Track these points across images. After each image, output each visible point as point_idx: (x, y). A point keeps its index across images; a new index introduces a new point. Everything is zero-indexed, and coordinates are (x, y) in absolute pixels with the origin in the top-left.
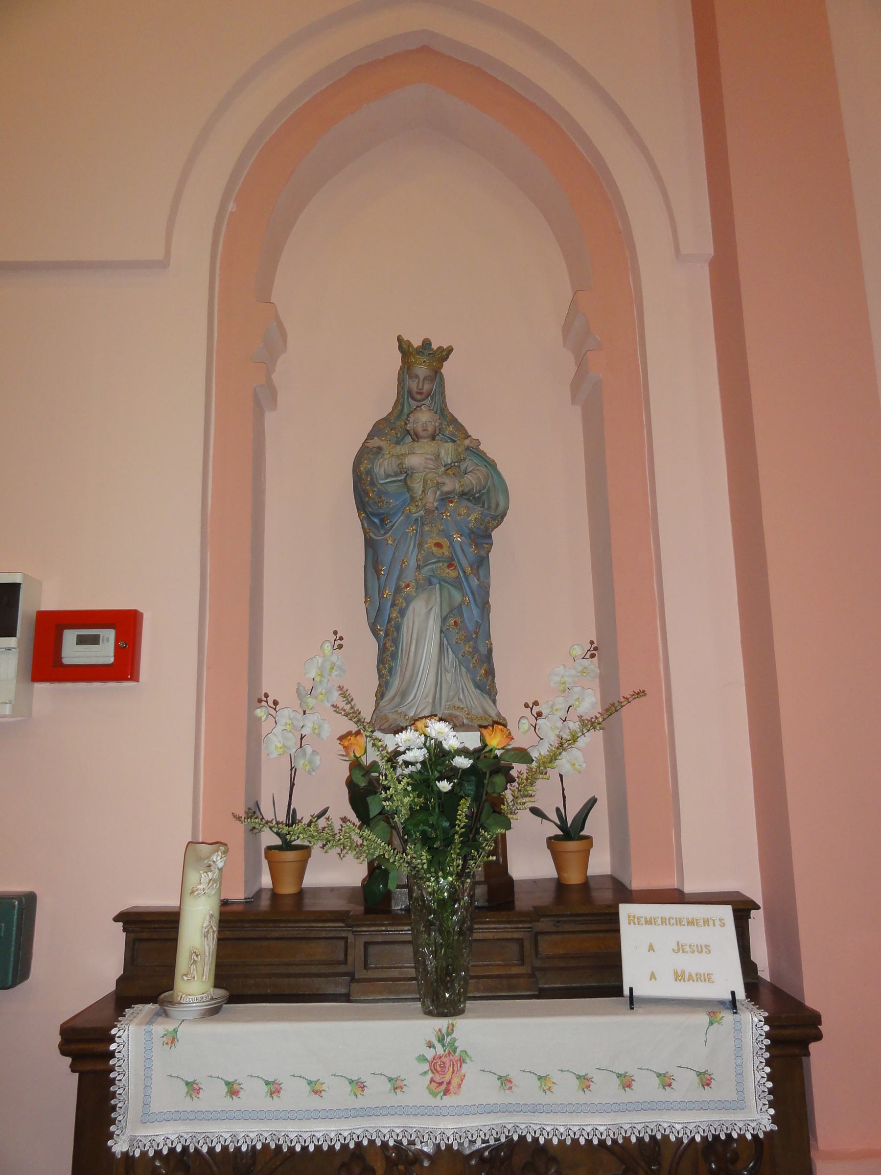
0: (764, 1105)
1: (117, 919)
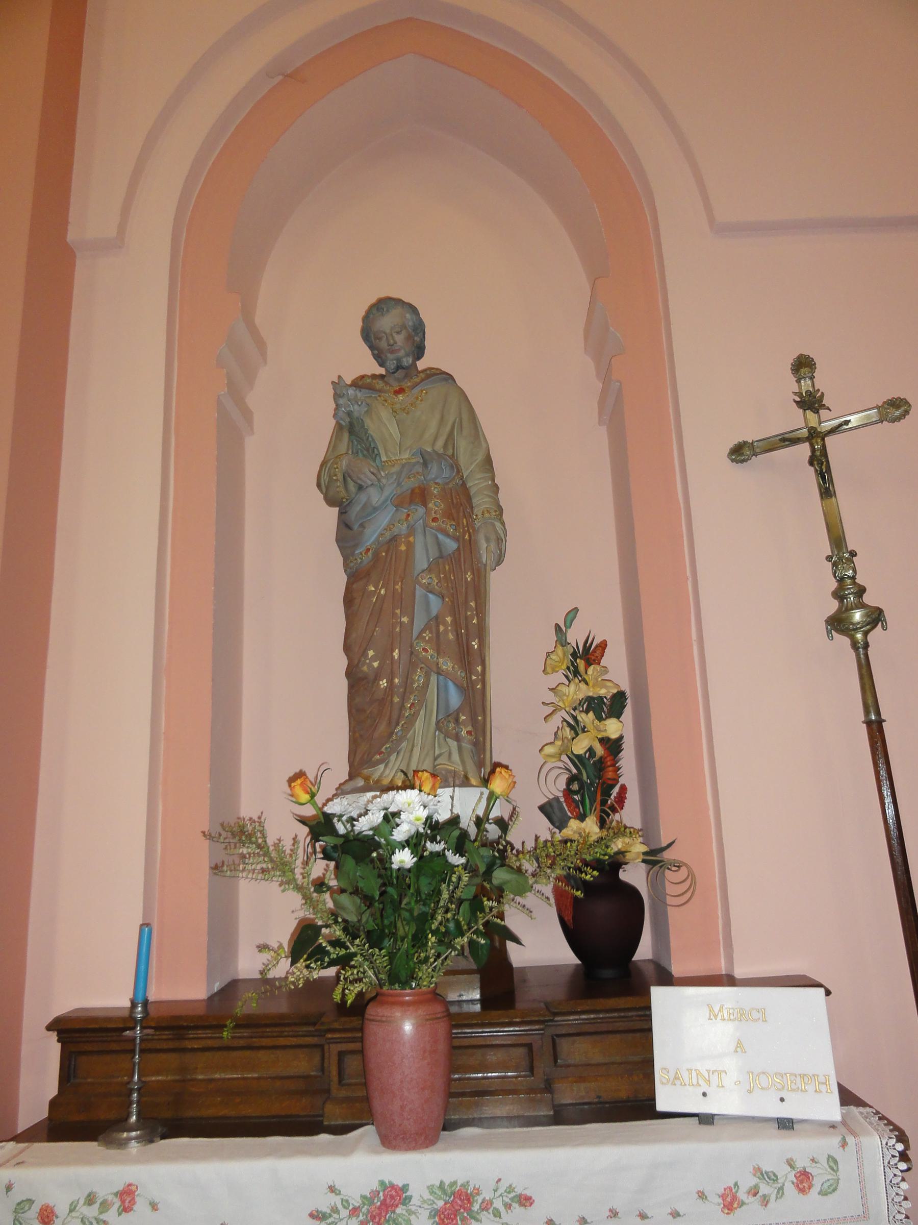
0: (893, 1156)
1: (49, 1028)
